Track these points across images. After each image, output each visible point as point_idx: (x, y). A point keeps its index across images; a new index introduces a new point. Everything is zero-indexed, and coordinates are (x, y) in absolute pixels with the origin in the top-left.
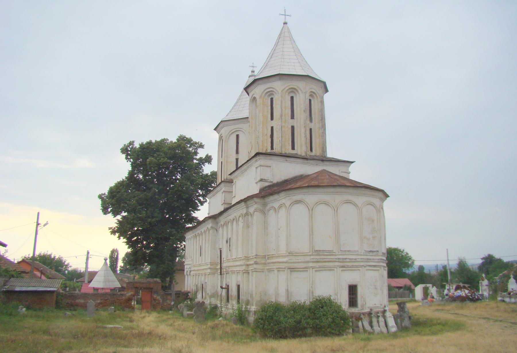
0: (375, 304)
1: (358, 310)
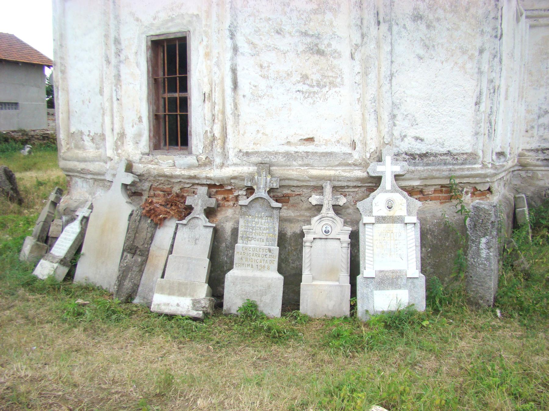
0: (311, 140)
1: (190, 167)
